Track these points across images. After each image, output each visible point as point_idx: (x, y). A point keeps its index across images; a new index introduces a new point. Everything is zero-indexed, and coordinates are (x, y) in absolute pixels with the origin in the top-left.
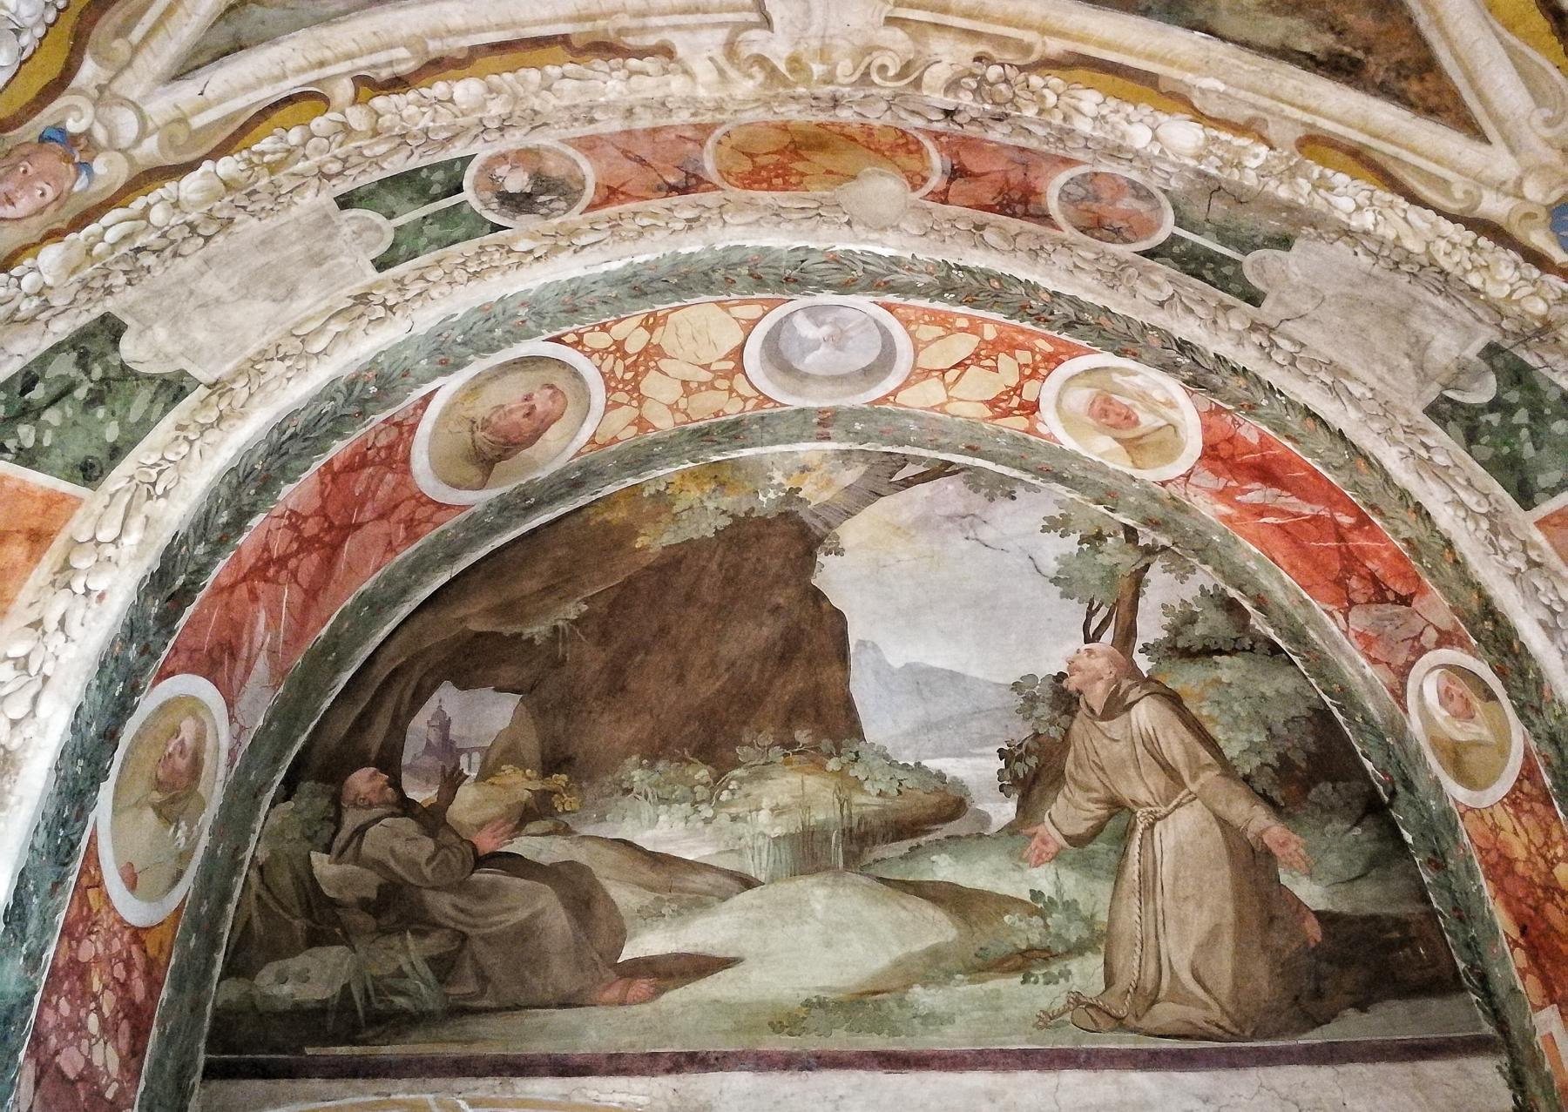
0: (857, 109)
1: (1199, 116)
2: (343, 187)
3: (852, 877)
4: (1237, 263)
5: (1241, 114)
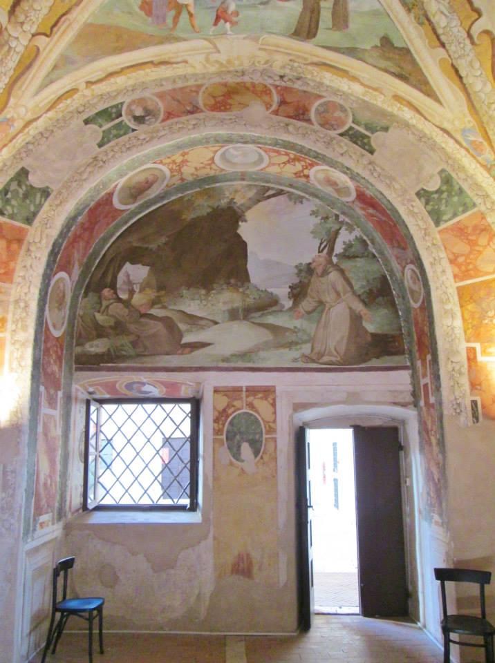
1: (362, 84)
2: (85, 116)
3: (245, 322)
4: (369, 137)
5: (375, 86)
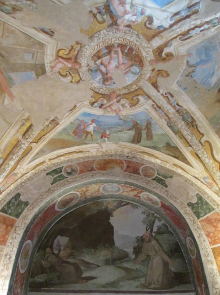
0: (115, 157)
1: (160, 160)
2: (47, 172)
4: (165, 181)
